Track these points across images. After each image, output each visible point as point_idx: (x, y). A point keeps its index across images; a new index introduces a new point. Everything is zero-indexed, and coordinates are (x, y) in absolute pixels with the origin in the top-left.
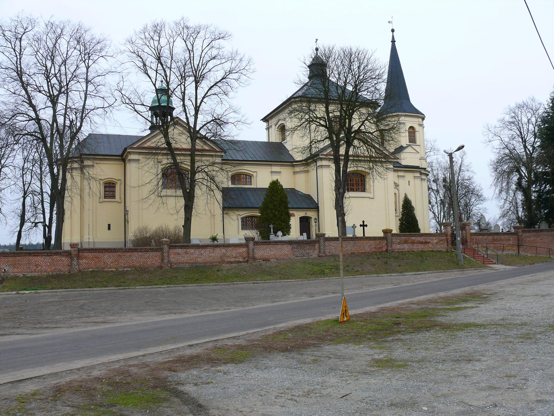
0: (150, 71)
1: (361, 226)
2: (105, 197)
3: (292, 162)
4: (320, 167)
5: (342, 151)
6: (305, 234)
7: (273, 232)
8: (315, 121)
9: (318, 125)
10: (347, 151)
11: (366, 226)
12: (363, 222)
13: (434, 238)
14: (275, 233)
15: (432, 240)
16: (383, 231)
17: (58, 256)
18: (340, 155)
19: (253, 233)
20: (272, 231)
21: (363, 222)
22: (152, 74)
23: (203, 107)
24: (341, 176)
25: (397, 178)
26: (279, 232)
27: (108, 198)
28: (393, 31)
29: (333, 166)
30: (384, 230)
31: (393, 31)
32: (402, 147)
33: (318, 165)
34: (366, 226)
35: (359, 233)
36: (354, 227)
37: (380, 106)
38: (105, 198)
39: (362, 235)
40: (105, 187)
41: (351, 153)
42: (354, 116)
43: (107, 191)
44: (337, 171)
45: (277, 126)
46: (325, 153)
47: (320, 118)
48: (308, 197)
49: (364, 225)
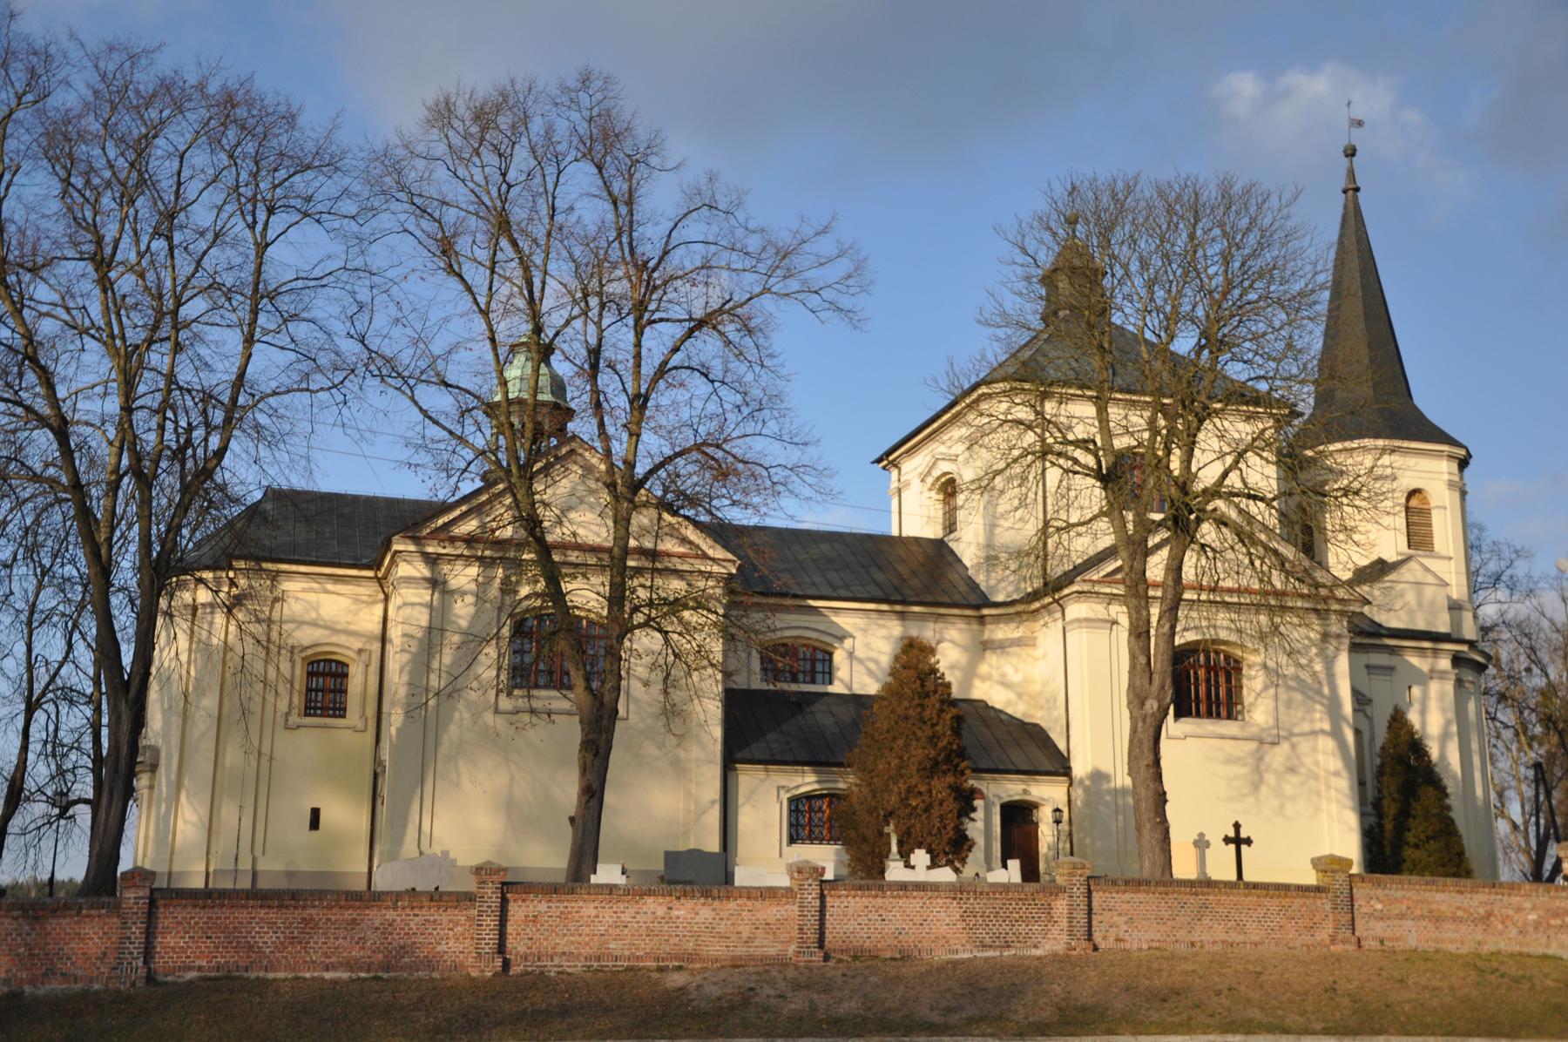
0: (469, 271)
1: (1227, 840)
2: (309, 710)
3: (978, 607)
4: (1077, 625)
5: (1156, 567)
6: (1014, 865)
7: (900, 852)
8: (1059, 454)
9: (1067, 471)
10: (1175, 568)
11: (1248, 842)
12: (1237, 826)
13: (1528, 905)
14: (905, 855)
15: (1519, 909)
16: (1318, 864)
17: (68, 920)
18: (1148, 585)
19: (826, 857)
20: (894, 848)
21: (1237, 826)
22: (478, 277)
23: (663, 397)
24: (1152, 652)
25: (1365, 670)
26: (916, 851)
27: (321, 716)
28: (1351, 152)
29: (1120, 613)
30: (1319, 859)
31: (1351, 152)
32: (1381, 562)
33: (1068, 618)
34: (1248, 842)
35: (1221, 866)
36: (1201, 844)
37: (1301, 414)
38: (306, 715)
39: (1233, 877)
40: (310, 674)
41: (1189, 573)
42: (1201, 436)
43: (317, 690)
44: (1139, 633)
45: (930, 480)
46: (1095, 578)
47: (1078, 443)
48: (1035, 735)
49: (1238, 841)
